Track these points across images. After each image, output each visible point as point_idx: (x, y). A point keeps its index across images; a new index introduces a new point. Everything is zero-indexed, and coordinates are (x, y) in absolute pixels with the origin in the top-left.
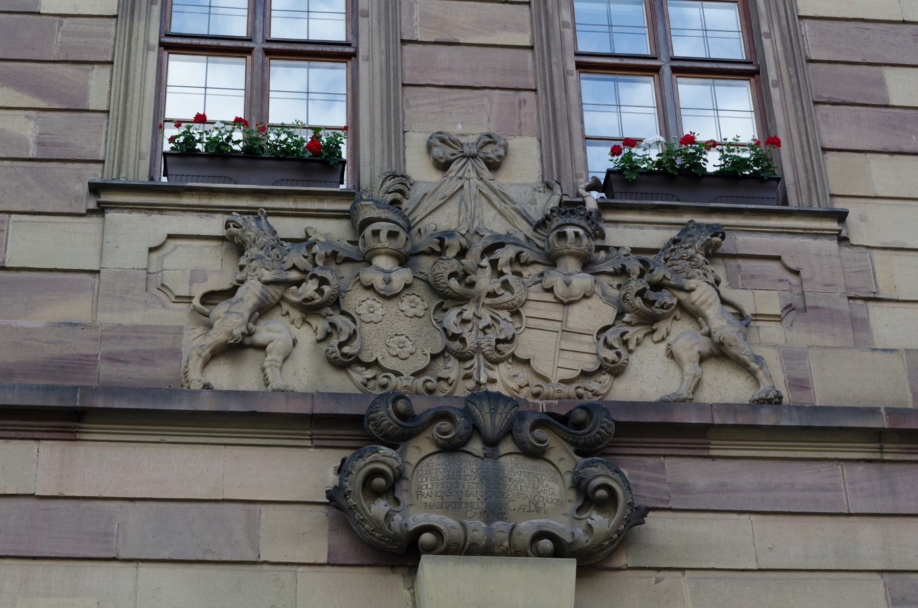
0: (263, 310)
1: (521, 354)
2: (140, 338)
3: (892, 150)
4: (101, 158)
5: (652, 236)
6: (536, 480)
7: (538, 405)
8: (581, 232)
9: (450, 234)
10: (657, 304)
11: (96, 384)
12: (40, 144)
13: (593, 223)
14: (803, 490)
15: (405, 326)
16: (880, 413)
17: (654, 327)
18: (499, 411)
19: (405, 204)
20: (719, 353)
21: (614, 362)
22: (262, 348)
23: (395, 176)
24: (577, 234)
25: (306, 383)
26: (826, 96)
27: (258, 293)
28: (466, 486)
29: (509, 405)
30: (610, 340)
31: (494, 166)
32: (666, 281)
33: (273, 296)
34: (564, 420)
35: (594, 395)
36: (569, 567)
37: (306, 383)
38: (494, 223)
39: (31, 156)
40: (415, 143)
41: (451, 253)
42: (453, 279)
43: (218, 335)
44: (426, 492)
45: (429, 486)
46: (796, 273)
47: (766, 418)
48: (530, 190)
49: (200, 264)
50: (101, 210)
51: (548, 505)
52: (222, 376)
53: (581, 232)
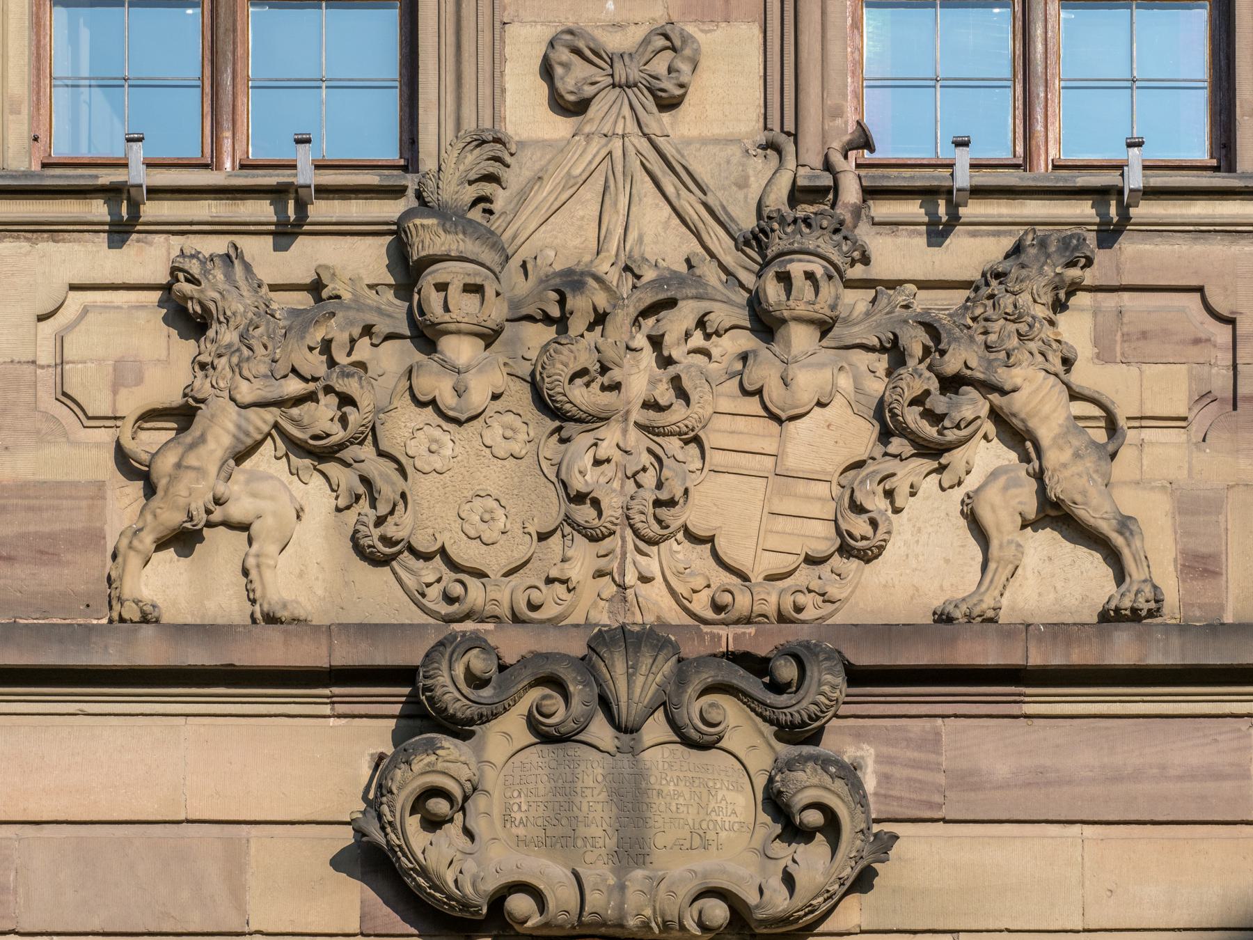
1: (700, 530)
2: (30, 509)
6: (705, 791)
10: (947, 423)
14: (1180, 778)
15: (493, 477)
17: (943, 461)
18: (643, 670)
19: (501, 199)
20: (1055, 514)
24: (810, 276)
25: (320, 592)
28: (585, 807)
30: (860, 497)
32: (969, 372)
37: (320, 592)
38: (661, 240)
43: (173, 518)
44: (518, 816)
45: (524, 807)
47: (1123, 650)
48: (735, 152)
51: (723, 834)
52: (162, 583)
53: (818, 268)
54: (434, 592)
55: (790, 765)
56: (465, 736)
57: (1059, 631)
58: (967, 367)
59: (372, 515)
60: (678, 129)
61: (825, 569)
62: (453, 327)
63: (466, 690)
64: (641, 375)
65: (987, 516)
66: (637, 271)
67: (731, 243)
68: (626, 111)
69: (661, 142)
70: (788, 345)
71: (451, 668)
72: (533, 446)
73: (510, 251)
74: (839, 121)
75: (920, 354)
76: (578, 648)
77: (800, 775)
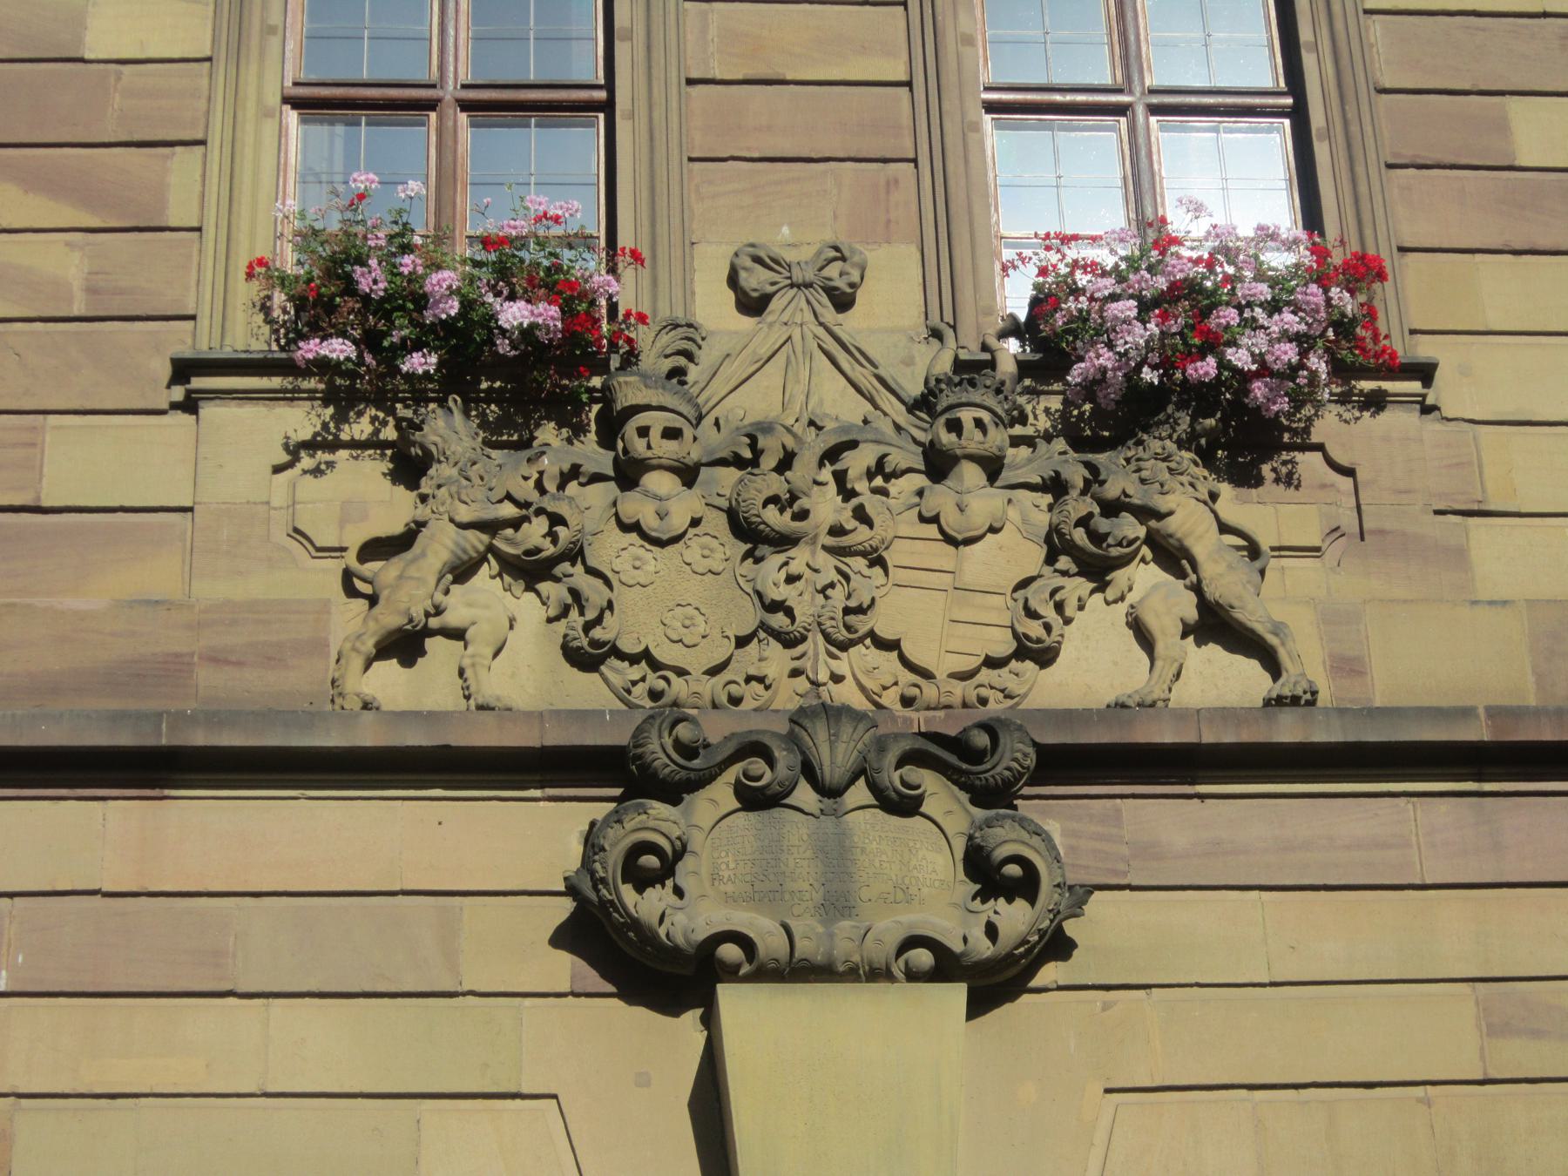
0: (462, 571)
1: (886, 633)
3: (1518, 247)
4: (191, 312)
7: (912, 721)
8: (986, 417)
9: (767, 428)
10: (1110, 540)
11: (194, 705)
12: (92, 290)
13: (1006, 398)
15: (694, 589)
16: (1477, 717)
18: (845, 738)
19: (693, 373)
20: (1214, 624)
21: (1039, 641)
22: (458, 634)
23: (676, 326)
24: (979, 423)
26: (1407, 155)
27: (451, 545)
28: (791, 863)
29: (861, 727)
30: (1033, 604)
31: (843, 302)
33: (474, 547)
34: (957, 744)
35: (1006, 697)
36: (956, 995)
38: (840, 405)
39: (76, 312)
41: (768, 462)
42: (771, 506)
43: (389, 618)
44: (726, 874)
45: (732, 865)
46: (1349, 472)
47: (1288, 730)
50: (190, 405)
51: (925, 890)
52: (389, 683)
53: (986, 417)
54: (640, 690)
55: (989, 824)
56: (675, 801)
57: (1225, 714)
58: (1127, 496)
59: (581, 621)
60: (851, 324)
61: (1004, 671)
62: (654, 462)
63: (675, 756)
64: (826, 507)
65: (1151, 621)
66: (819, 423)
67: (903, 408)
68: (803, 304)
69: (836, 329)
70: (961, 479)
71: (660, 737)
72: (729, 565)
73: (704, 411)
74: (992, 318)
75: (1081, 485)
76: (783, 727)
77: (998, 830)
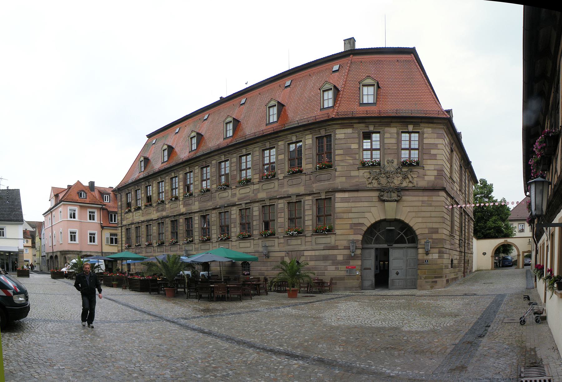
5: (406, 170)
20: (410, 182)
38: (392, 169)
40: (386, 160)
49: (367, 175)
52: (369, 186)
